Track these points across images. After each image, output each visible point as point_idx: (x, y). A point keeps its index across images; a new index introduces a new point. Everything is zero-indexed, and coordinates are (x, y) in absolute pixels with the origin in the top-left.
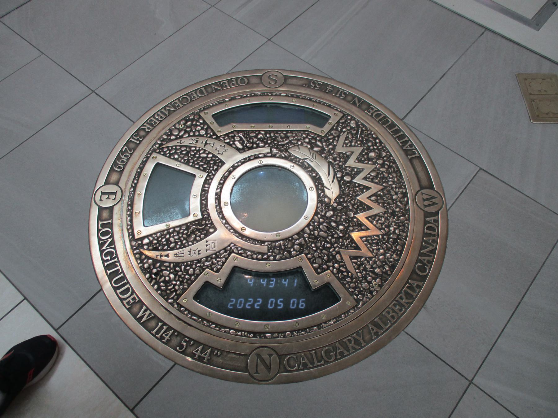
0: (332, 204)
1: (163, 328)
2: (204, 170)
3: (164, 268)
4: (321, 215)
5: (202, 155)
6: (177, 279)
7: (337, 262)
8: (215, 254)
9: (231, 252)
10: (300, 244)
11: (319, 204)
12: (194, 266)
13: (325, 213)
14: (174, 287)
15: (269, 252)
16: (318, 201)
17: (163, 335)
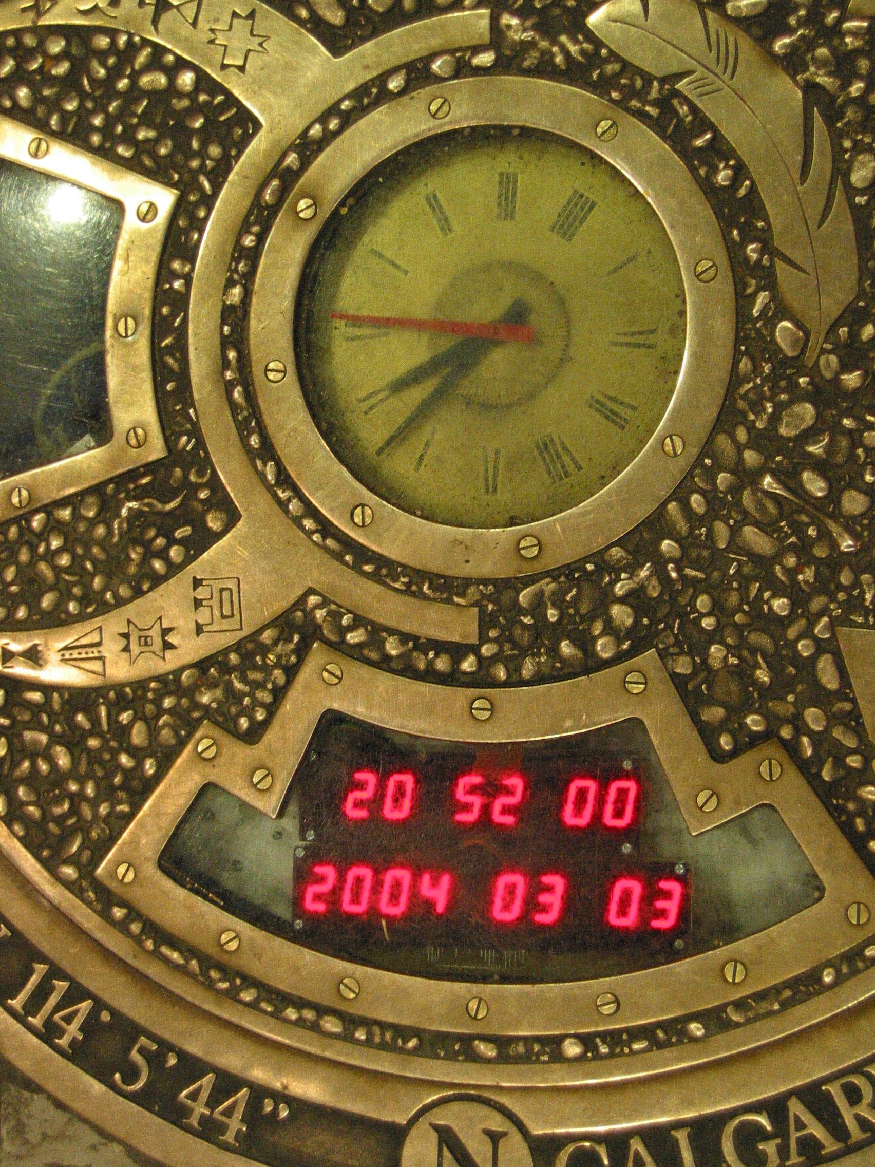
0: (810, 357)
1: (52, 989)
2: (158, 173)
3: (27, 716)
4: (750, 428)
5: (145, 80)
6: (83, 768)
7: (819, 696)
8: (238, 647)
9: (310, 633)
10: (635, 599)
11: (745, 364)
12: (149, 708)
13: (775, 419)
14: (74, 810)
15: (484, 639)
16: (738, 341)
17: (57, 1017)
